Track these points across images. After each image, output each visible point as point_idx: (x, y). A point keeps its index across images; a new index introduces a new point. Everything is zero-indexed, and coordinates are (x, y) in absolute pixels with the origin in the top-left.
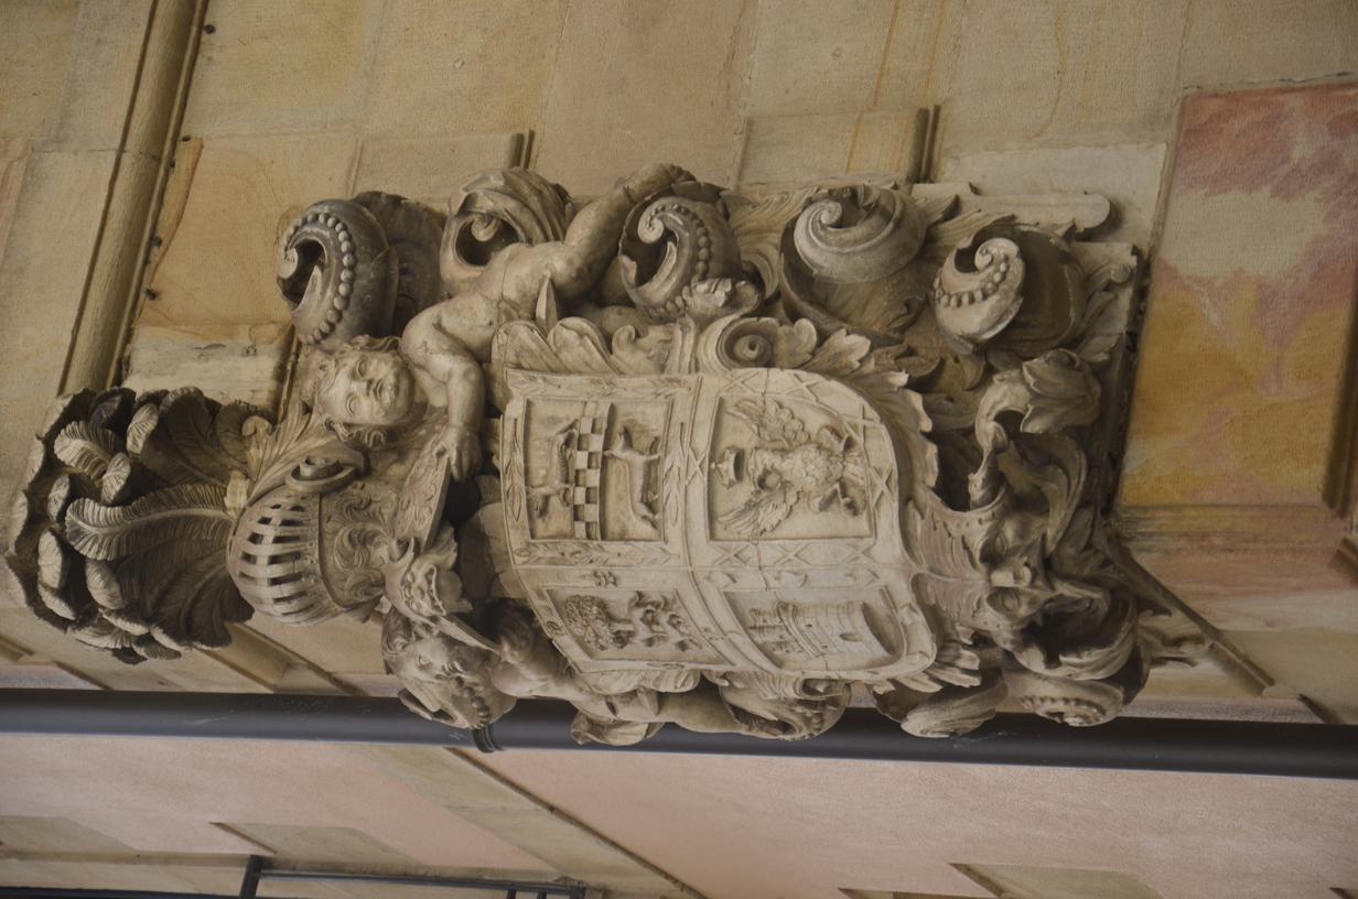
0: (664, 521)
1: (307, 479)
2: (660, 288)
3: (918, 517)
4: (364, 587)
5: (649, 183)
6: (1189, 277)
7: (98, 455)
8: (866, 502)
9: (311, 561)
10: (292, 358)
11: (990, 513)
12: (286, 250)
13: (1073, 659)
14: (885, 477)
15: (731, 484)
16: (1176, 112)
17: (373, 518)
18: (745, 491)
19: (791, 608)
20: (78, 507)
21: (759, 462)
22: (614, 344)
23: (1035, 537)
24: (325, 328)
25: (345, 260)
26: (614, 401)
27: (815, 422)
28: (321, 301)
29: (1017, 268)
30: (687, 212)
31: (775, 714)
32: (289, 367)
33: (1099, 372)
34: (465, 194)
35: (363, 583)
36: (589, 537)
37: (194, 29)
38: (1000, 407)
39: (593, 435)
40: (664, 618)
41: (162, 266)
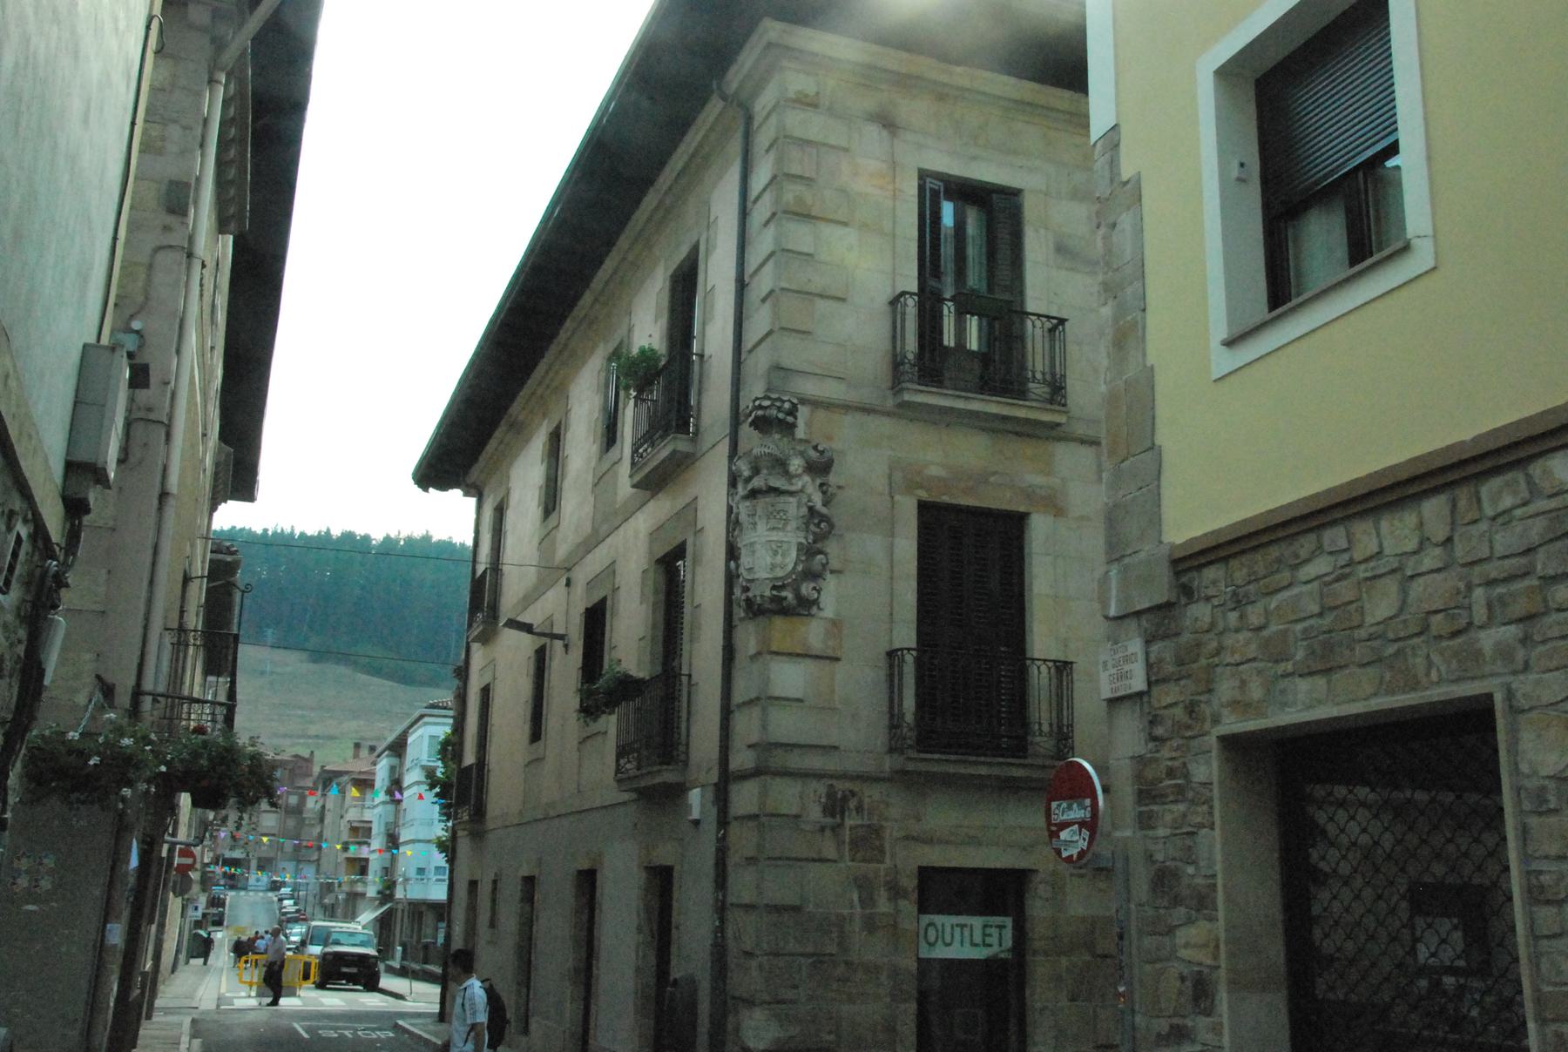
2: (812, 527)
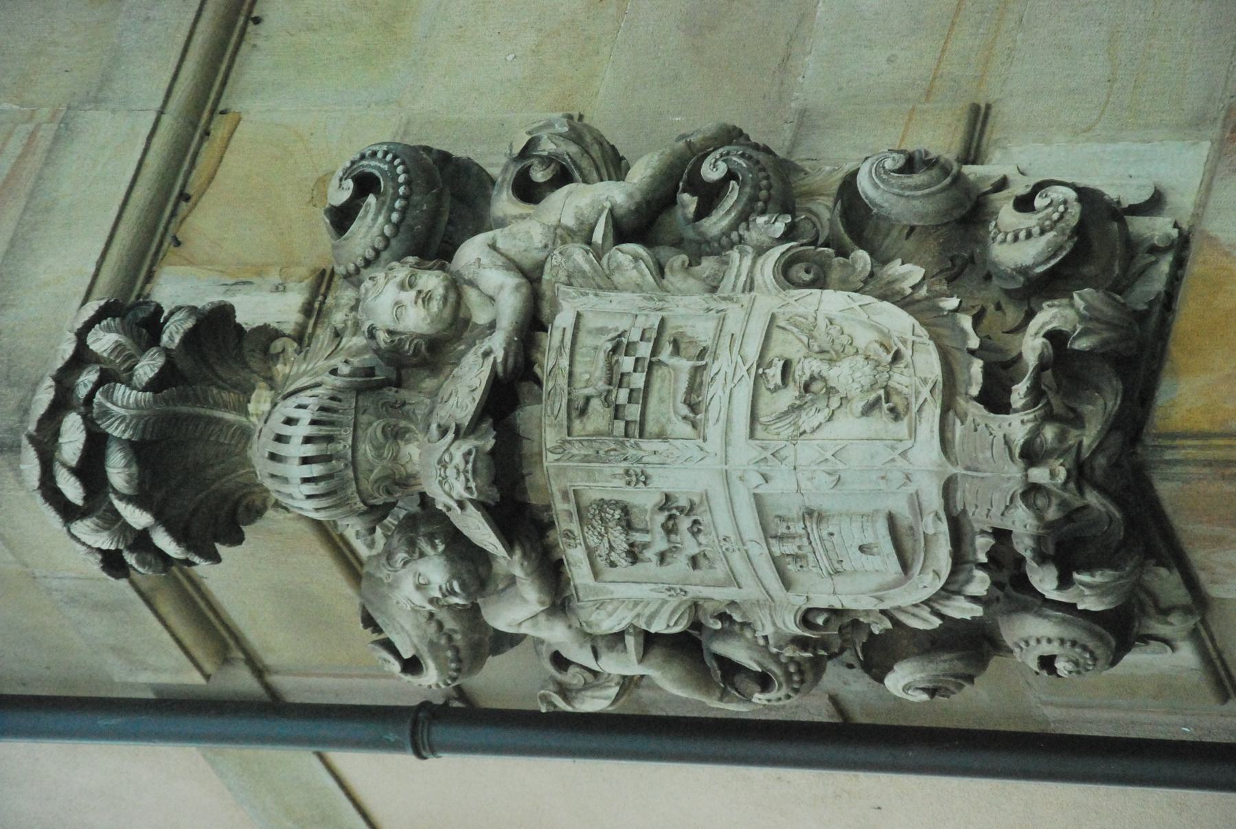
0: (707, 420)
1: (345, 376)
2: (716, 223)
3: (958, 422)
4: (387, 483)
5: (709, 139)
6: (1230, 245)
7: (131, 348)
8: (908, 407)
9: (343, 446)
10: (320, 298)
11: (1031, 416)
12: (341, 180)
13: (1085, 578)
14: (930, 386)
15: (776, 389)
16: (1223, 114)
17: (407, 417)
18: (789, 396)
19: (816, 515)
20: (108, 389)
21: (806, 368)
22: (666, 270)
23: (1072, 441)
24: (370, 254)
25: (401, 190)
26: (664, 314)
27: (865, 338)
28: (370, 228)
29: (1075, 210)
30: (750, 158)
31: (760, 664)
32: (317, 305)
33: (1141, 317)
34: (528, 137)
35: (386, 477)
36: (626, 435)
37: (241, 20)
38: (1049, 327)
40: (685, 523)
41: (189, 219)
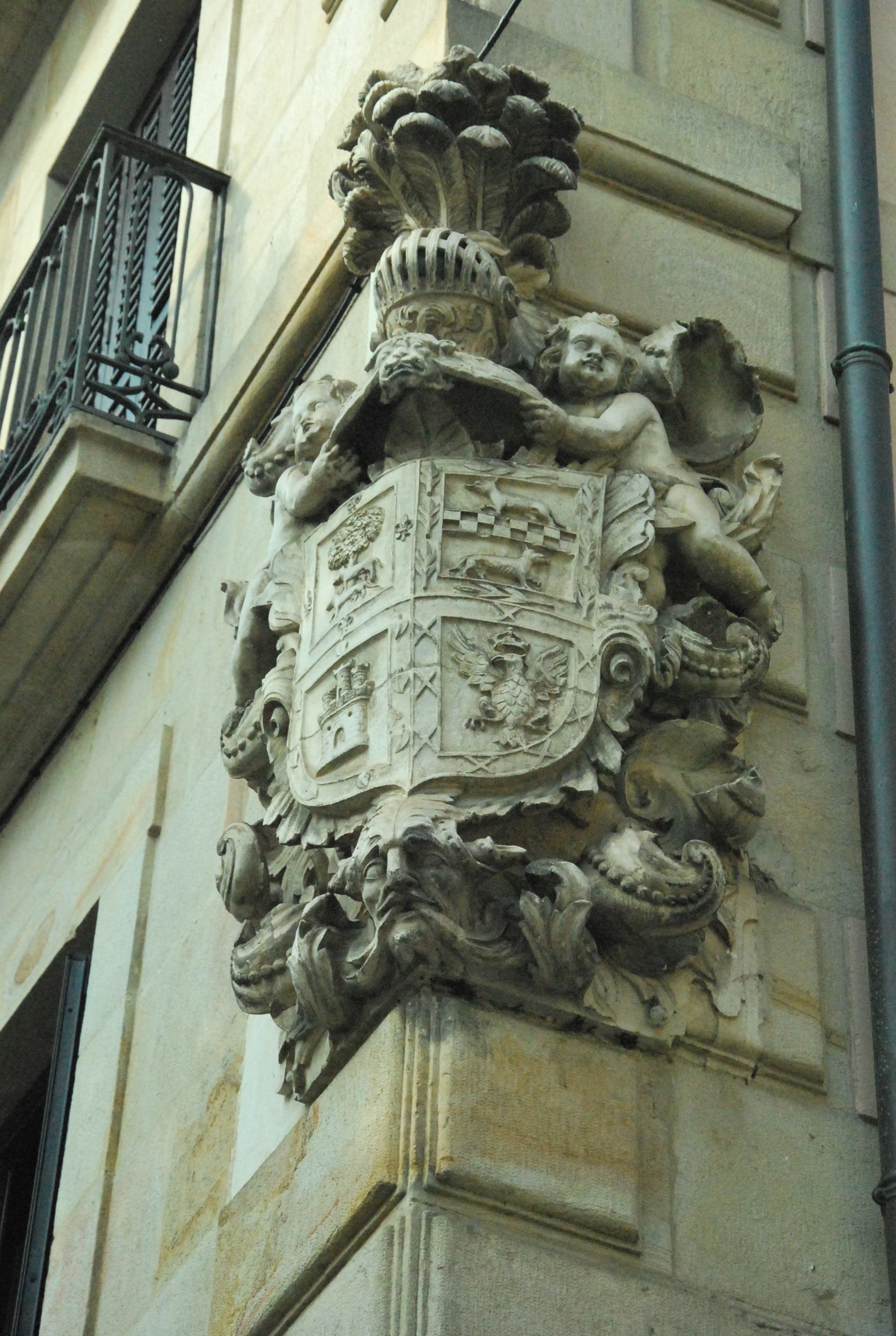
39: (542, 537)
